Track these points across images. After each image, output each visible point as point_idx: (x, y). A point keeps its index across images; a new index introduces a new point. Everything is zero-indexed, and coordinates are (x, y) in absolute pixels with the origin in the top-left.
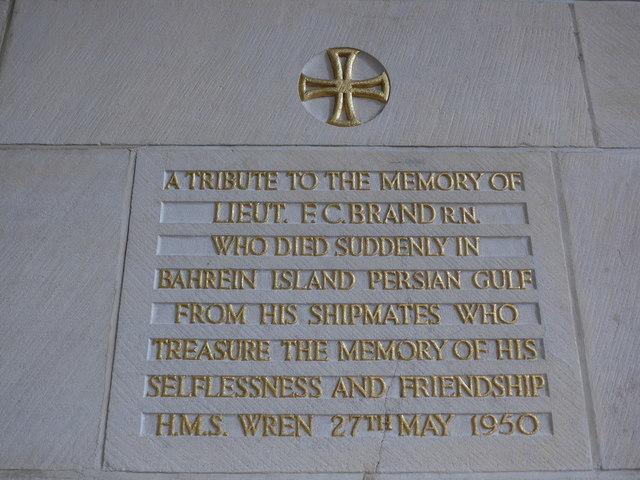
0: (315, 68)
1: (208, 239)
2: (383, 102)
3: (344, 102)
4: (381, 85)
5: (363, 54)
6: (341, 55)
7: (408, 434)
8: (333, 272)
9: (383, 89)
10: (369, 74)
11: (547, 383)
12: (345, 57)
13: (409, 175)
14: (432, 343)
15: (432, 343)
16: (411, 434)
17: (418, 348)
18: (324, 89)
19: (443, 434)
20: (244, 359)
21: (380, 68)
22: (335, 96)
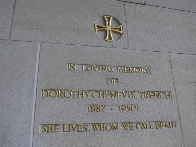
0: (98, 21)
1: (121, 124)
2: (120, 34)
3: (109, 35)
4: (120, 29)
5: (114, 18)
6: (107, 18)
7: (74, 131)
8: (97, 66)
9: (120, 30)
10: (116, 26)
11: (138, 109)
12: (109, 19)
13: (127, 68)
14: (146, 69)
15: (146, 69)
16: (76, 131)
17: (142, 70)
19: (172, 98)
20: (113, 130)
21: (120, 24)
22: (106, 31)
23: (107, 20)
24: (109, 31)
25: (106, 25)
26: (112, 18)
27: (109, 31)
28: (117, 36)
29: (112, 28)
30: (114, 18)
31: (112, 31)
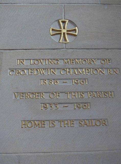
2: (75, 35)
4: (75, 30)
9: (76, 32)
12: (64, 22)
18: (58, 33)
22: (61, 34)
23: (61, 23)
24: (64, 33)
25: (61, 28)
26: (67, 21)
27: (64, 33)
28: (73, 38)
29: (67, 31)
30: (70, 21)
31: (67, 34)
